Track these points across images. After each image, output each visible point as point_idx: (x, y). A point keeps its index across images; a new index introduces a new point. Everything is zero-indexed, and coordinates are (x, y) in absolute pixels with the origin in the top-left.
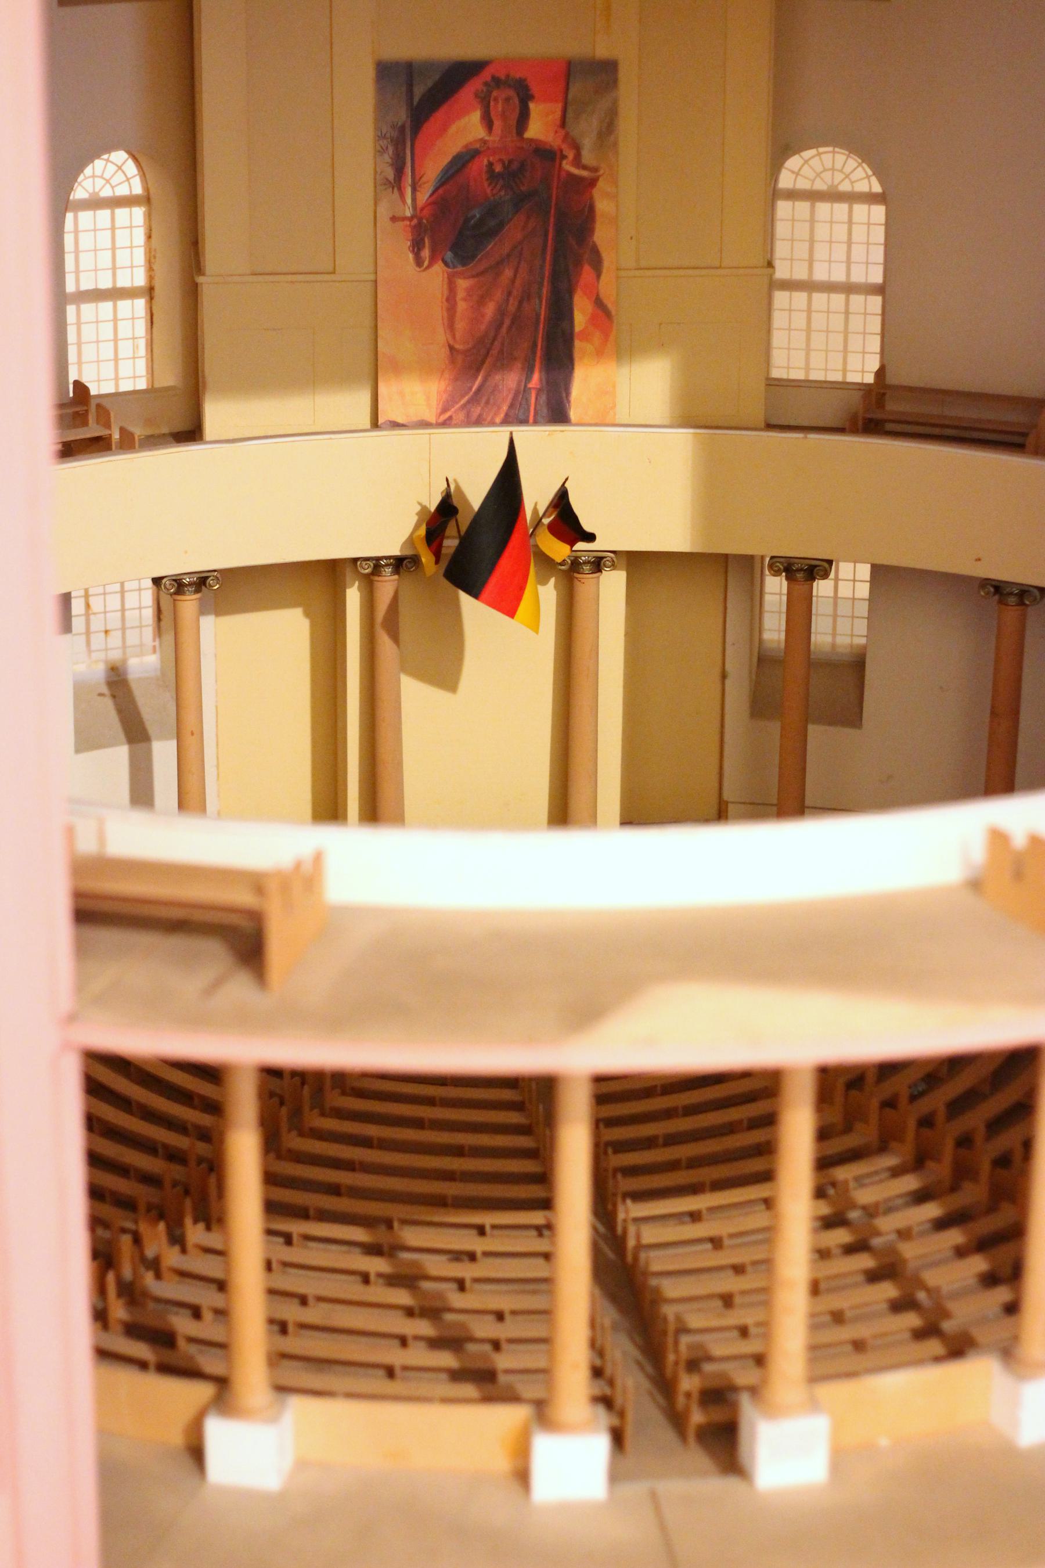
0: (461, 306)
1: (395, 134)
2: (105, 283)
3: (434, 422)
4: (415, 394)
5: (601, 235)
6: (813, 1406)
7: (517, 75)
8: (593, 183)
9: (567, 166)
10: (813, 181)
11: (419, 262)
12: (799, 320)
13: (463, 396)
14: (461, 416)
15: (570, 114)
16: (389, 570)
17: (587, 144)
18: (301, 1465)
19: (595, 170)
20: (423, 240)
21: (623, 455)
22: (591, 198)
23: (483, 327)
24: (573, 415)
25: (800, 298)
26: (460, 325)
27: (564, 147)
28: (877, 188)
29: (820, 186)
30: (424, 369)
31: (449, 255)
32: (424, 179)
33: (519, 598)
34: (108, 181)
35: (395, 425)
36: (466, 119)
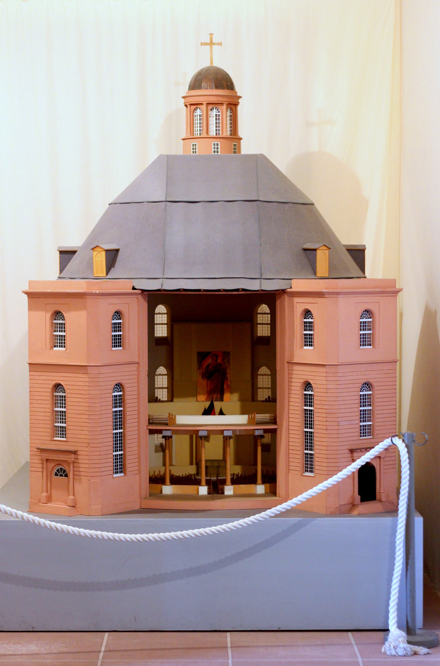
0: (209, 386)
2: (161, 386)
4: (202, 398)
5: (228, 376)
6: (232, 487)
9: (223, 366)
12: (262, 393)
24: (224, 400)
25: (261, 390)
28: (270, 373)
29: (264, 373)
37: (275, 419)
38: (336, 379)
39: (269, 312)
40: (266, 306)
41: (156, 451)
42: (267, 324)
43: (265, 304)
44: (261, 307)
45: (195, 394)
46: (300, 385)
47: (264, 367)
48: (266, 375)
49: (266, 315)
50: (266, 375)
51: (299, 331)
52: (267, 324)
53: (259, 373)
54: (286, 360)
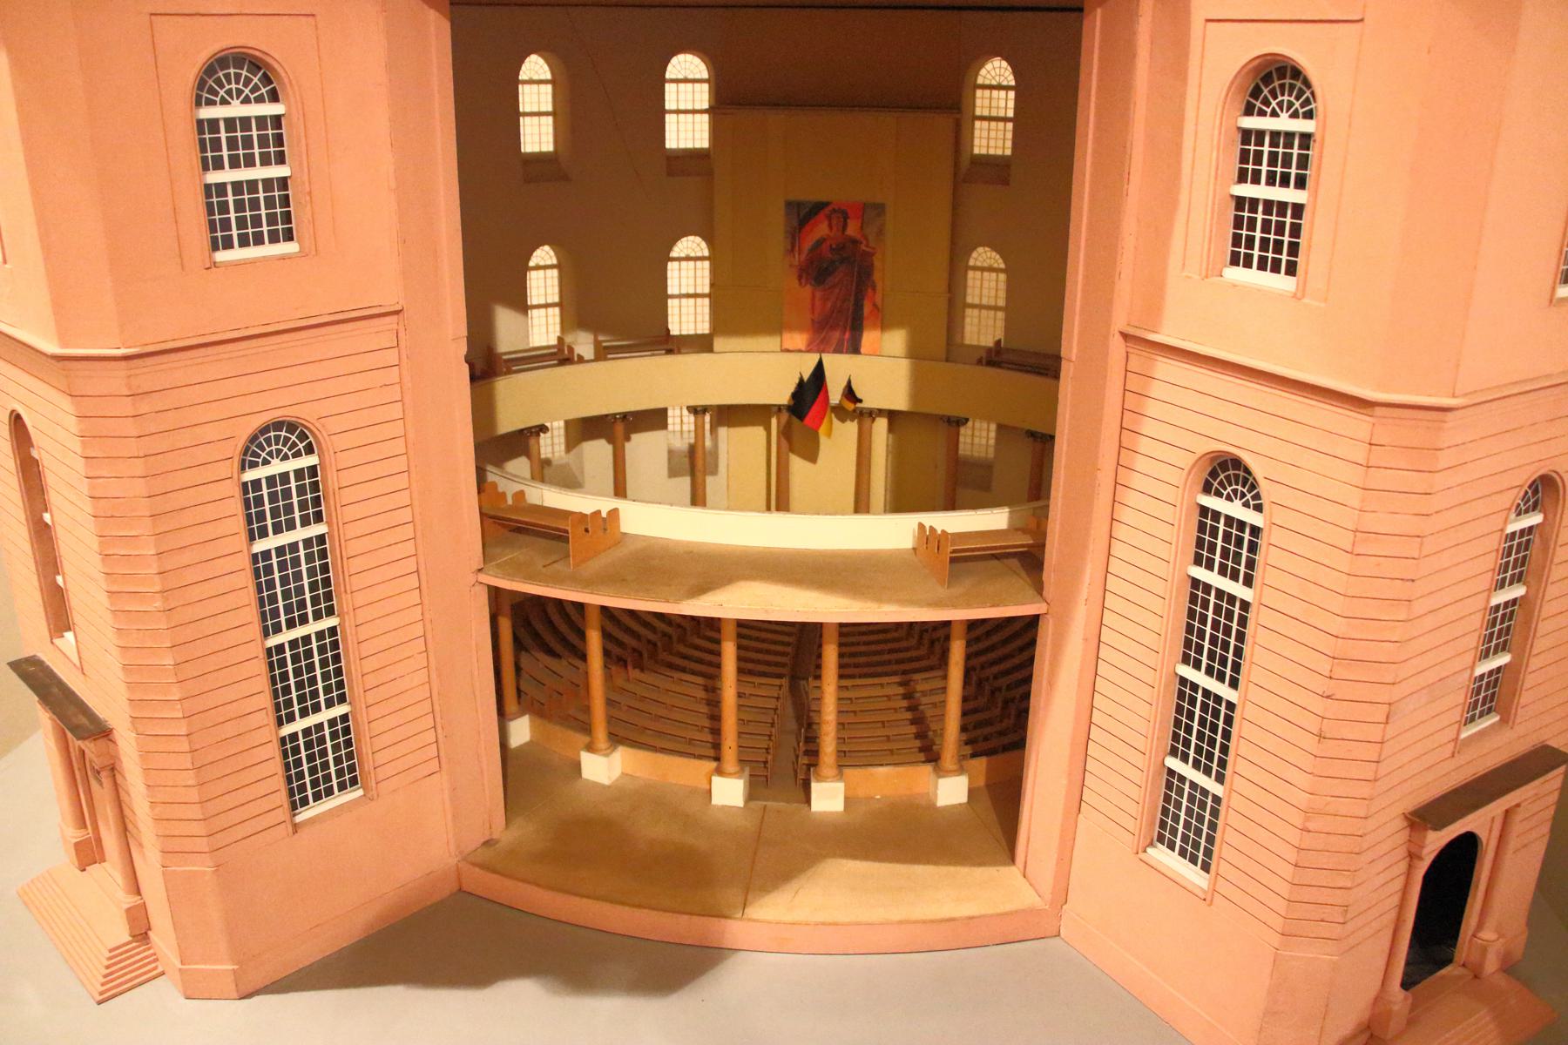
4: (798, 339)
5: (877, 276)
17: (871, 238)
18: (624, 775)
21: (880, 370)
28: (1002, 266)
35: (788, 351)
38: (1417, 482)
39: (1013, 83)
40: (1004, 64)
41: (673, 472)
44: (989, 66)
45: (774, 327)
46: (1187, 461)
47: (981, 250)
48: (991, 269)
50: (991, 269)
51: (1206, 181)
54: (1120, 322)
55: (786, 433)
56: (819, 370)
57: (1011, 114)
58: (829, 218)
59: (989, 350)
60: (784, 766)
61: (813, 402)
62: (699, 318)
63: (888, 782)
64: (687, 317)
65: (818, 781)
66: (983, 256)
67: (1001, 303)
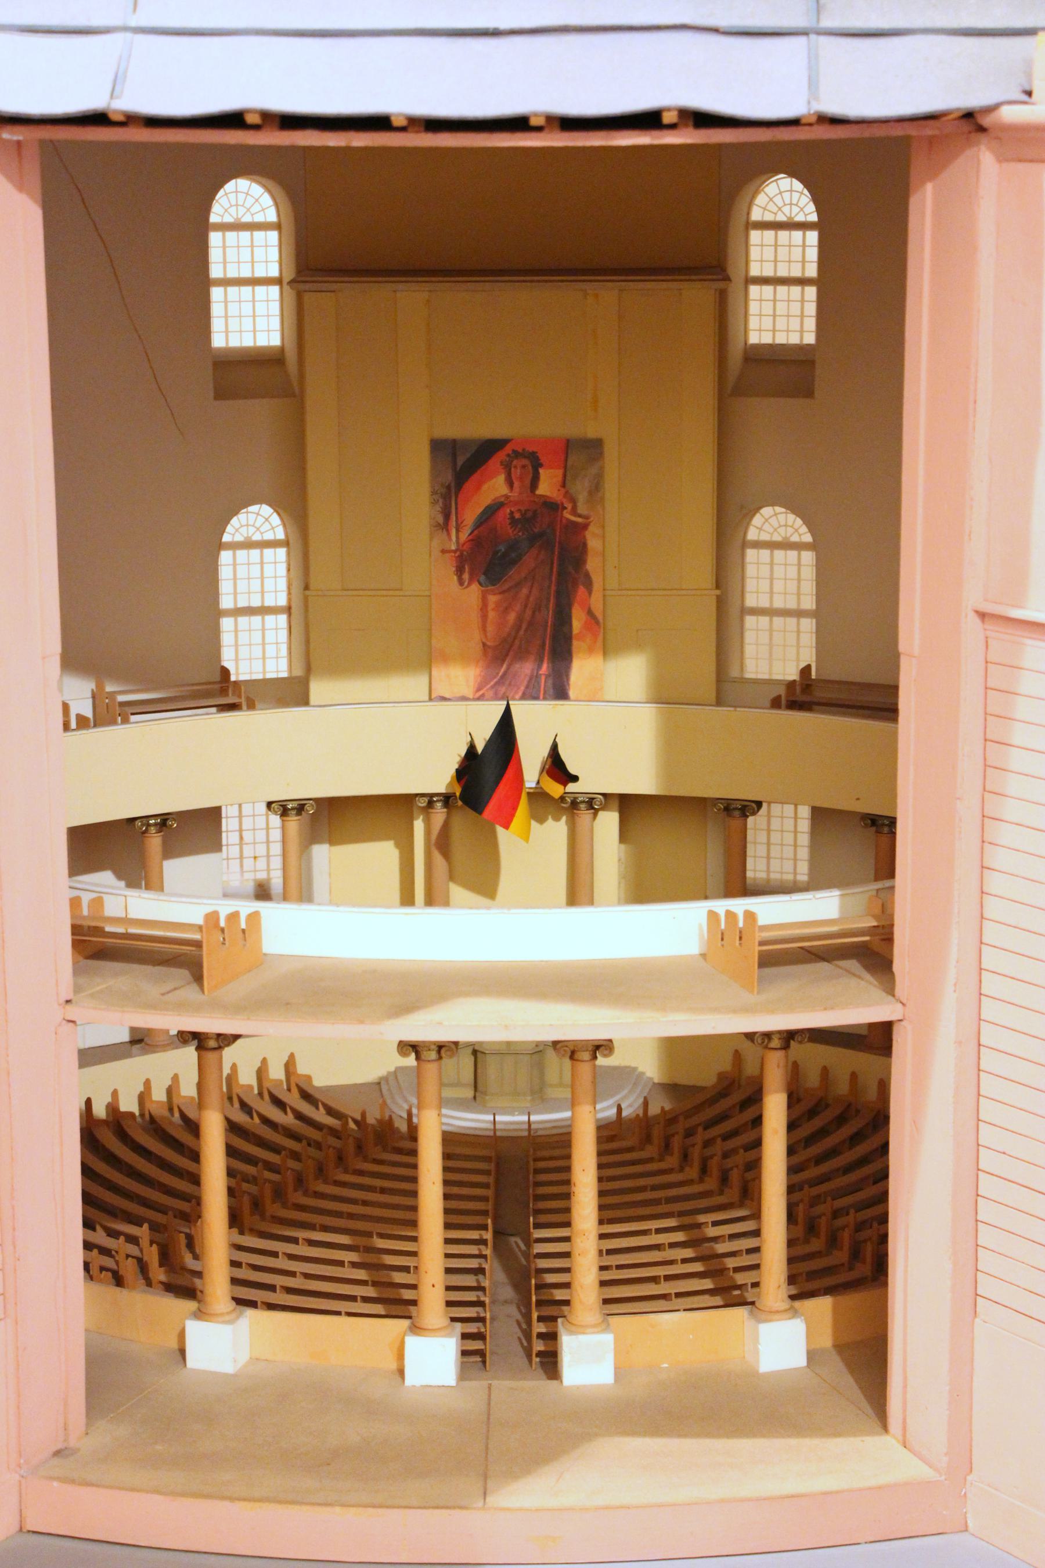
0: (492, 615)
1: (444, 491)
2: (256, 603)
3: (471, 697)
4: (460, 677)
5: (592, 564)
6: (604, 1326)
7: (530, 449)
8: (585, 527)
9: (567, 515)
10: (772, 534)
11: (461, 583)
13: (492, 679)
14: (491, 693)
15: (568, 478)
16: (439, 805)
17: (582, 498)
18: (254, 1360)
19: (587, 517)
20: (463, 567)
21: (607, 723)
22: (584, 537)
23: (507, 630)
24: (572, 693)
26: (490, 628)
27: (564, 501)
28: (808, 538)
29: (777, 538)
30: (464, 659)
31: (482, 578)
32: (465, 523)
33: (512, 816)
34: (258, 529)
35: (443, 699)
36: (494, 480)
37: (885, 934)
39: (814, 218)
40: (798, 185)
42: (802, 282)
43: (792, 174)
47: (767, 511)
49: (797, 235)
52: (802, 282)
53: (752, 535)
55: (442, 843)
56: (506, 727)
57: (812, 271)
58: (508, 468)
59: (791, 685)
60: (517, 1319)
61: (497, 783)
62: (271, 651)
63: (684, 1336)
64: (257, 649)
65: (571, 1333)
66: (772, 522)
67: (809, 603)
